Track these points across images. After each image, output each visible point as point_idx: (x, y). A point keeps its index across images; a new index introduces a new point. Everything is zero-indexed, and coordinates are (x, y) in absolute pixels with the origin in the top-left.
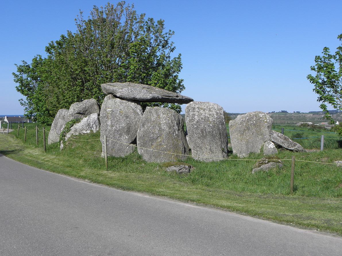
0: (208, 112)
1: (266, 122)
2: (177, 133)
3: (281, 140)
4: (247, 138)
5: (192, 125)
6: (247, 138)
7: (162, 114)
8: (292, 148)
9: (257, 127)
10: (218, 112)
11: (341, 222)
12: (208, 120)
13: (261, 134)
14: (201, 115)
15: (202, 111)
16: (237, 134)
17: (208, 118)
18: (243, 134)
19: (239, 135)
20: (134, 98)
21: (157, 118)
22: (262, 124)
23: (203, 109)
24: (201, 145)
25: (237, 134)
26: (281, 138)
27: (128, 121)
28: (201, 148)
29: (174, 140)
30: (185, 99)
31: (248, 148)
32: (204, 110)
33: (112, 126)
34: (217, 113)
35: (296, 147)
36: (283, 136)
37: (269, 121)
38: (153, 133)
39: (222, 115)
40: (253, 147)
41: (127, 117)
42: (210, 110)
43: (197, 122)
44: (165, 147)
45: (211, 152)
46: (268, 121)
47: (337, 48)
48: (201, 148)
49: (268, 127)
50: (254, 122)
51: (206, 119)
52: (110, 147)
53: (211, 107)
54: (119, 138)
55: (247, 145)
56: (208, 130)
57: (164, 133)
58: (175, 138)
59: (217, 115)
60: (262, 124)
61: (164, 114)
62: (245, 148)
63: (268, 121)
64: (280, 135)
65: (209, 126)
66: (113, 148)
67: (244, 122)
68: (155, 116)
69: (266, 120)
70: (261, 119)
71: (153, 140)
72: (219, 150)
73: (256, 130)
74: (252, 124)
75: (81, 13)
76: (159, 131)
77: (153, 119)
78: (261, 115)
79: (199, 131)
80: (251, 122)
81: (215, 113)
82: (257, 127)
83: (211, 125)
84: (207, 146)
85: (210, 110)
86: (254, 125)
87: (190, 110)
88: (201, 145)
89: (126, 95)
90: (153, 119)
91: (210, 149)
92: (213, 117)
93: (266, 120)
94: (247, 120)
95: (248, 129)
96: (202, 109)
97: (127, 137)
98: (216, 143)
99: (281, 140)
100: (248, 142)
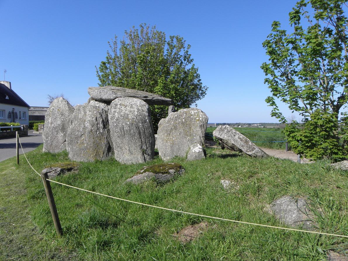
0: (129, 108)
1: (199, 120)
2: (101, 131)
3: (240, 143)
4: (174, 139)
5: (113, 123)
6: (174, 139)
7: (88, 112)
8: (250, 153)
9: (186, 126)
10: (140, 108)
11: (347, 228)
12: (127, 118)
13: (190, 135)
14: (122, 112)
15: (123, 108)
16: (164, 134)
17: (128, 115)
18: (170, 134)
19: (166, 135)
20: (101, 99)
21: (83, 115)
22: (193, 123)
23: (125, 105)
24: (121, 145)
25: (164, 134)
26: (241, 140)
27: (62, 118)
28: (121, 148)
29: (96, 139)
30: (156, 100)
31: (172, 151)
32: (126, 107)
33: (52, 124)
34: (138, 110)
35: (253, 152)
36: (244, 138)
37: (202, 119)
38: (78, 131)
39: (145, 113)
40: (179, 149)
41: (62, 115)
42: (132, 107)
43: (117, 120)
44: (86, 145)
45: (130, 153)
46: (201, 119)
47: (290, 26)
48: (121, 148)
49: (201, 126)
50: (183, 120)
51: (126, 117)
52: (49, 144)
53: (133, 103)
54: (56, 135)
55: (172, 147)
56: (126, 128)
57: (87, 130)
58: (97, 137)
59: (137, 112)
60: (193, 123)
61: (90, 111)
62: (169, 151)
63: (201, 119)
64: (241, 137)
65: (126, 124)
66: (52, 144)
67: (172, 119)
68: (83, 113)
69: (198, 118)
70: (192, 117)
71: (77, 138)
72: (138, 152)
73: (184, 130)
74: (180, 122)
75: (116, 37)
76: (83, 129)
77: (80, 116)
78: (193, 113)
79: (118, 130)
80: (179, 121)
81: (136, 110)
82: (186, 126)
83: (128, 123)
84: (127, 147)
85: (132, 107)
86: (182, 123)
87: (112, 107)
88: (121, 145)
89: (95, 96)
90: (80, 116)
91: (129, 150)
92: (133, 114)
93: (198, 118)
94: (176, 118)
95: (176, 128)
96: (123, 105)
97: (62, 134)
98: (135, 143)
99: (240, 143)
100: (173, 144)
